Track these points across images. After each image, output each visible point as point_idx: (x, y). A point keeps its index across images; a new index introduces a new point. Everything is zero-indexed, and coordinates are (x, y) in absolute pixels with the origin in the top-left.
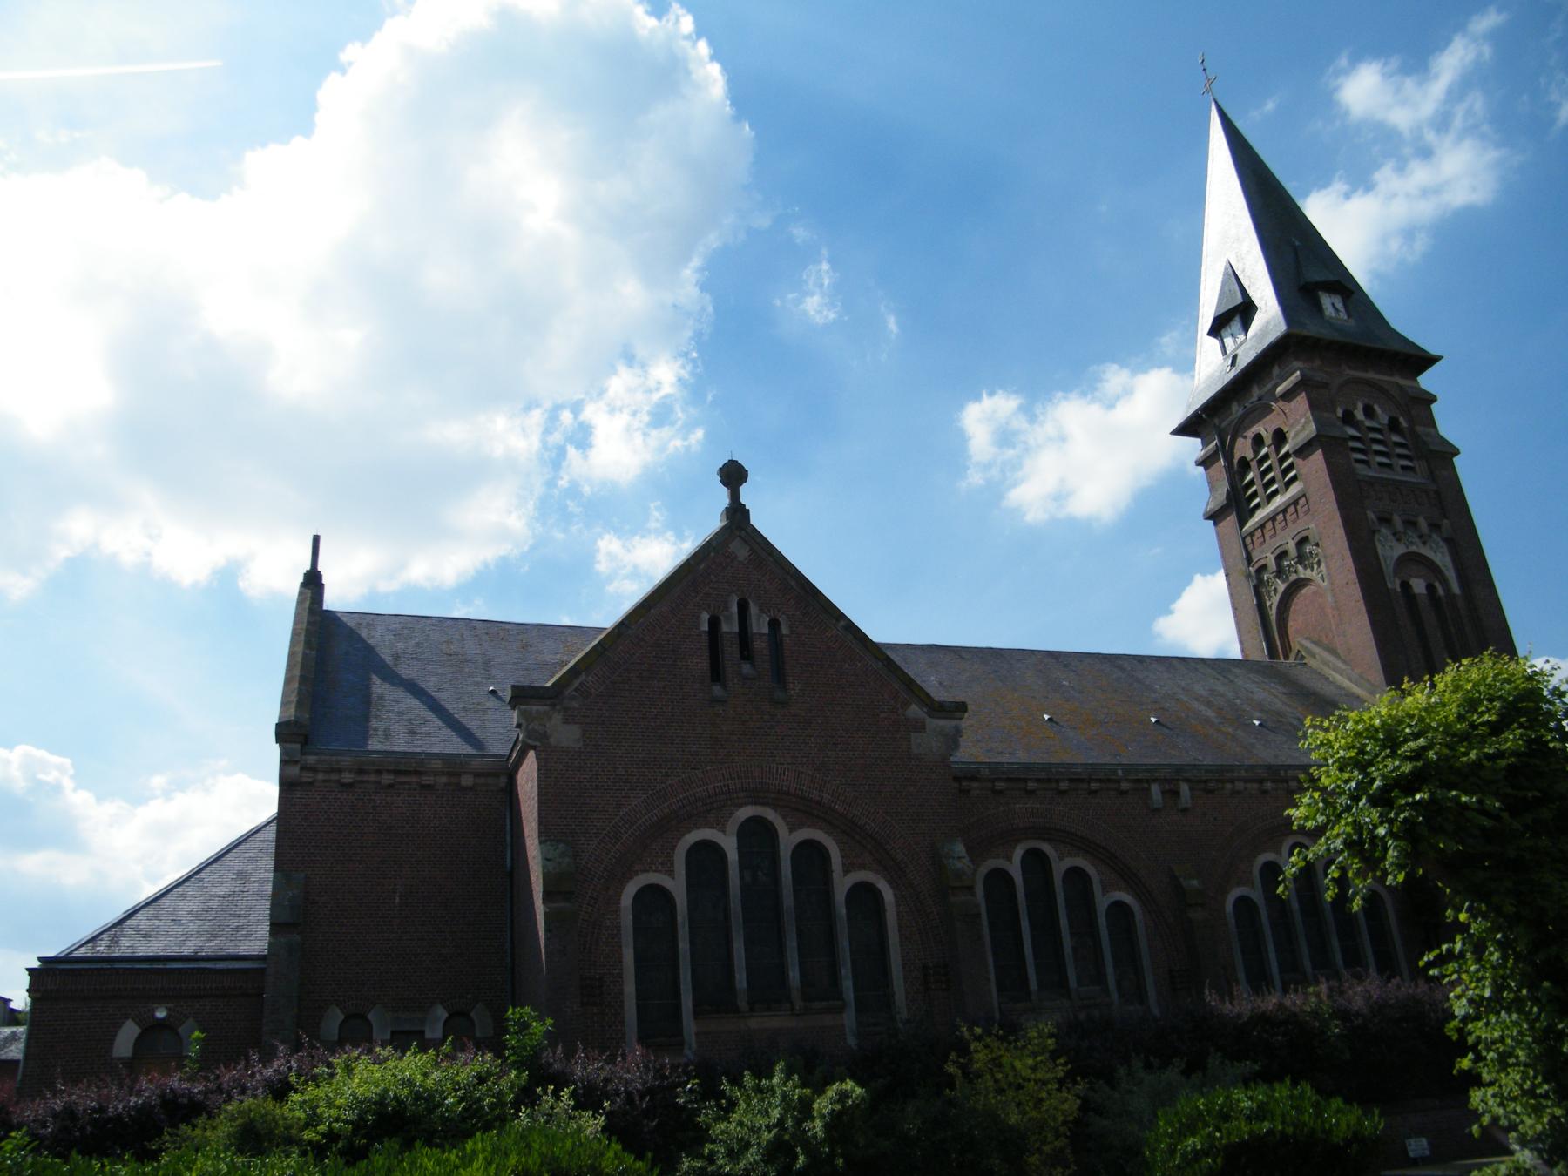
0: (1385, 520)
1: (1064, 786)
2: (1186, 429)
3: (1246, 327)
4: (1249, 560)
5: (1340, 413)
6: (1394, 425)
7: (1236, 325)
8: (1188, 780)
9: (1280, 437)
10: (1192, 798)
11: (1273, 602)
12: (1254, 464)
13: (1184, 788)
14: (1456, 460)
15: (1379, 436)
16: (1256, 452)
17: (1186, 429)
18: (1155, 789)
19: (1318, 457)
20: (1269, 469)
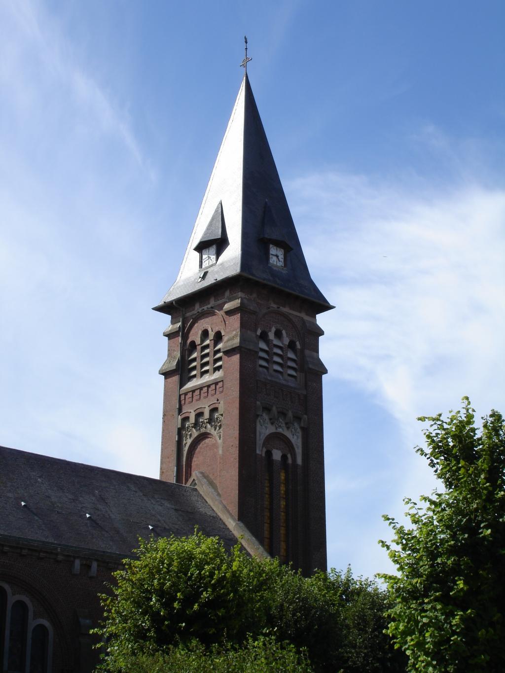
0: (267, 409)
1: (25, 552)
2: (165, 308)
3: (218, 254)
4: (180, 410)
5: (259, 332)
6: (292, 345)
7: (213, 250)
8: (97, 560)
9: (218, 337)
10: (98, 571)
11: (188, 442)
12: (199, 348)
13: (95, 565)
14: (324, 376)
15: (279, 352)
16: (202, 341)
17: (165, 308)
18: (77, 563)
19: (236, 358)
20: (207, 355)
